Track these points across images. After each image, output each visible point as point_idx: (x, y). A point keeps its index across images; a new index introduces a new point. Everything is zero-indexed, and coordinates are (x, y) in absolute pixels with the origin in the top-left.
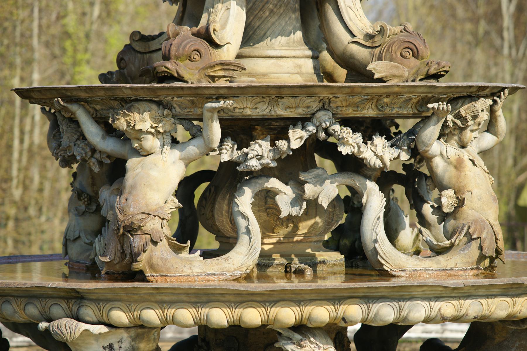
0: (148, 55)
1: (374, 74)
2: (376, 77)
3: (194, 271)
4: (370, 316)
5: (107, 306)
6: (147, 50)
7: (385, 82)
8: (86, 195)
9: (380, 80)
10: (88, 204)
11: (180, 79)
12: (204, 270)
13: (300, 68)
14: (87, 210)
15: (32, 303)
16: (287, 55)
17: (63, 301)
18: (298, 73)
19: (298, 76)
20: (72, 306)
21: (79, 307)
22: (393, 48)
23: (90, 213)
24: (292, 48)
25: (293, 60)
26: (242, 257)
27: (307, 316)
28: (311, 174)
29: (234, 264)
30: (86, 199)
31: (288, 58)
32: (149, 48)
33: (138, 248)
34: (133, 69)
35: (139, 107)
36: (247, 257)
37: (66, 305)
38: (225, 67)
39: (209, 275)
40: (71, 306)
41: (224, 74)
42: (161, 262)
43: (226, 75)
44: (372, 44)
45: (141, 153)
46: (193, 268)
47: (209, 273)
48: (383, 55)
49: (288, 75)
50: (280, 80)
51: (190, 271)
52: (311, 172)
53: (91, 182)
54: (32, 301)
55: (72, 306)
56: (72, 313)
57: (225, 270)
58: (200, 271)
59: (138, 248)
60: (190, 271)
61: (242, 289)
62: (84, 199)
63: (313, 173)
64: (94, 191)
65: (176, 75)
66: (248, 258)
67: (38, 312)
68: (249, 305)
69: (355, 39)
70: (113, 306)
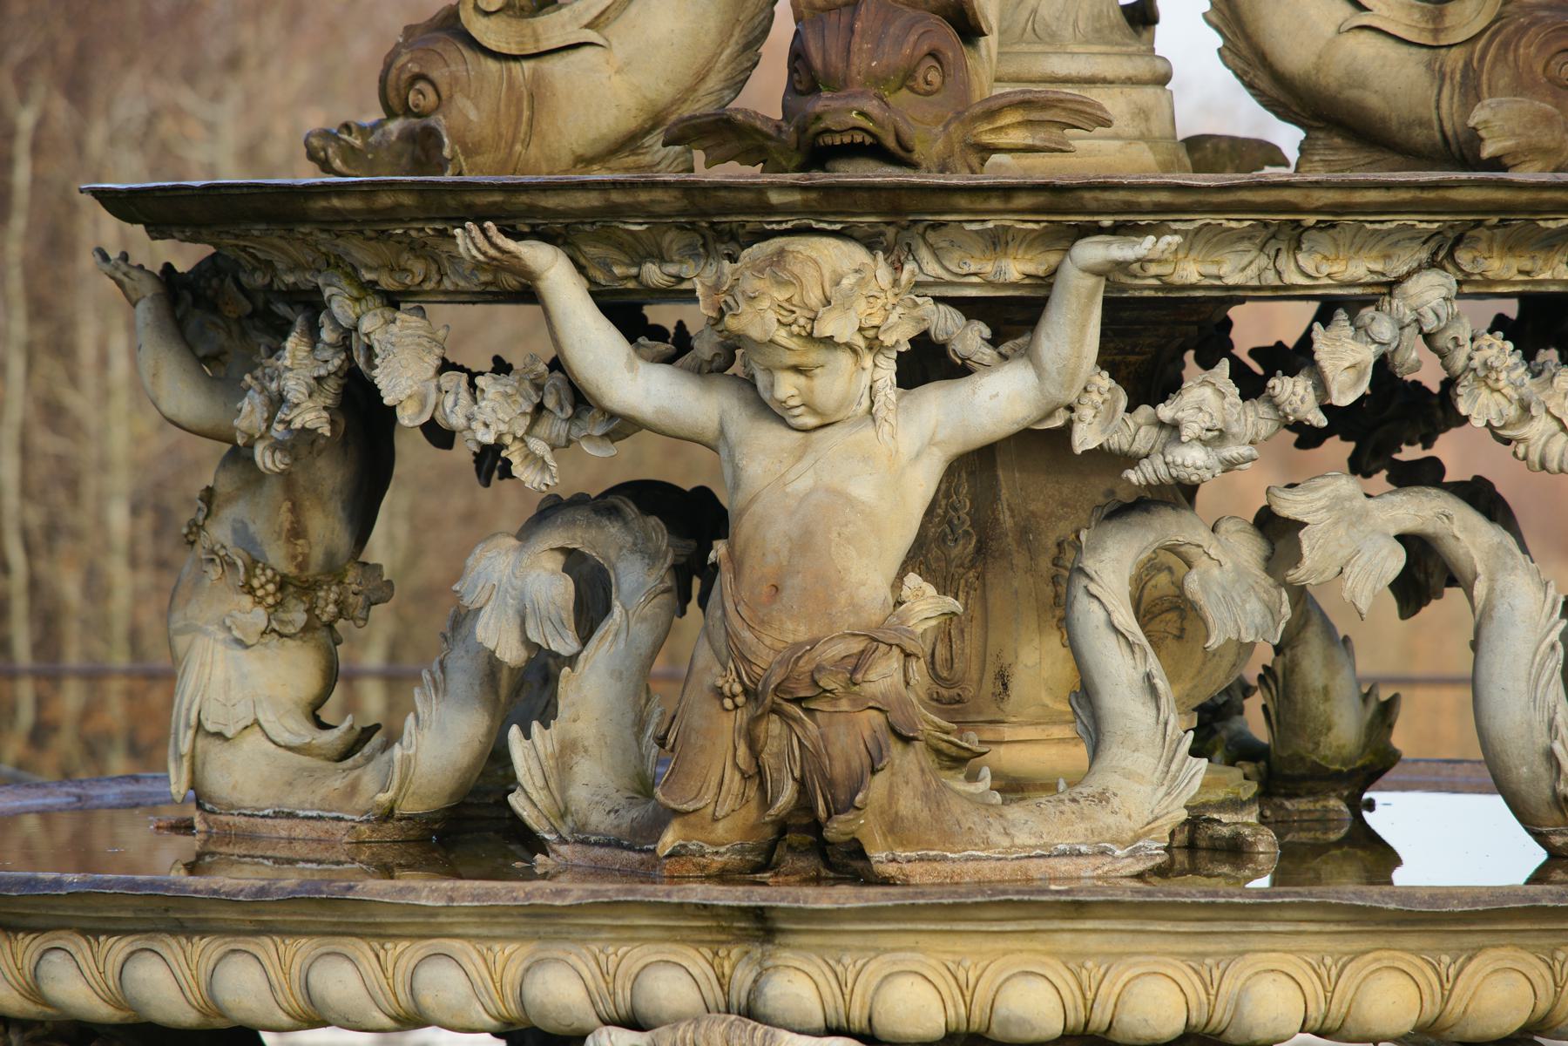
0: (527, 65)
1: (1482, 139)
2: (1487, 151)
3: (1018, 841)
4: (619, 998)
5: (873, 966)
6: (531, 50)
7: (1505, 169)
8: (269, 573)
9: (1496, 163)
10: (279, 604)
11: (900, 157)
12: (1046, 839)
13: (1147, 119)
14: (275, 625)
15: (557, 960)
16: (1110, 75)
17: (691, 952)
18: (1142, 138)
19: (1143, 146)
20: (734, 967)
21: (760, 974)
22: (1521, 51)
23: (281, 635)
24: (1116, 49)
25: (1127, 90)
26: (1149, 789)
27: (744, 1002)
28: (1316, 495)
29: (1129, 817)
30: (271, 587)
31: (1112, 82)
32: (537, 41)
33: (848, 762)
34: (473, 115)
35: (814, 254)
36: (1163, 790)
37: (707, 967)
38: (1035, 115)
39: (1063, 854)
40: (727, 971)
41: (1029, 141)
42: (926, 813)
43: (1038, 143)
44: (1436, 38)
45: (793, 422)
46: (1012, 831)
47: (1061, 847)
48: (1484, 78)
49: (1118, 143)
50: (1092, 160)
51: (1006, 842)
52: (1316, 489)
53: (287, 525)
54: (561, 955)
55: (734, 967)
56: (727, 994)
57: (1108, 837)
58: (1032, 841)
59: (848, 762)
60: (1006, 842)
61: (1392, 906)
62: (262, 586)
63: (1322, 492)
64: (294, 557)
65: (891, 143)
66: (1168, 794)
67: (583, 994)
68: (1386, 963)
69: (1365, 19)
70: (896, 969)
